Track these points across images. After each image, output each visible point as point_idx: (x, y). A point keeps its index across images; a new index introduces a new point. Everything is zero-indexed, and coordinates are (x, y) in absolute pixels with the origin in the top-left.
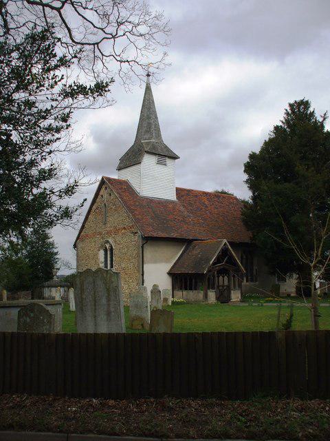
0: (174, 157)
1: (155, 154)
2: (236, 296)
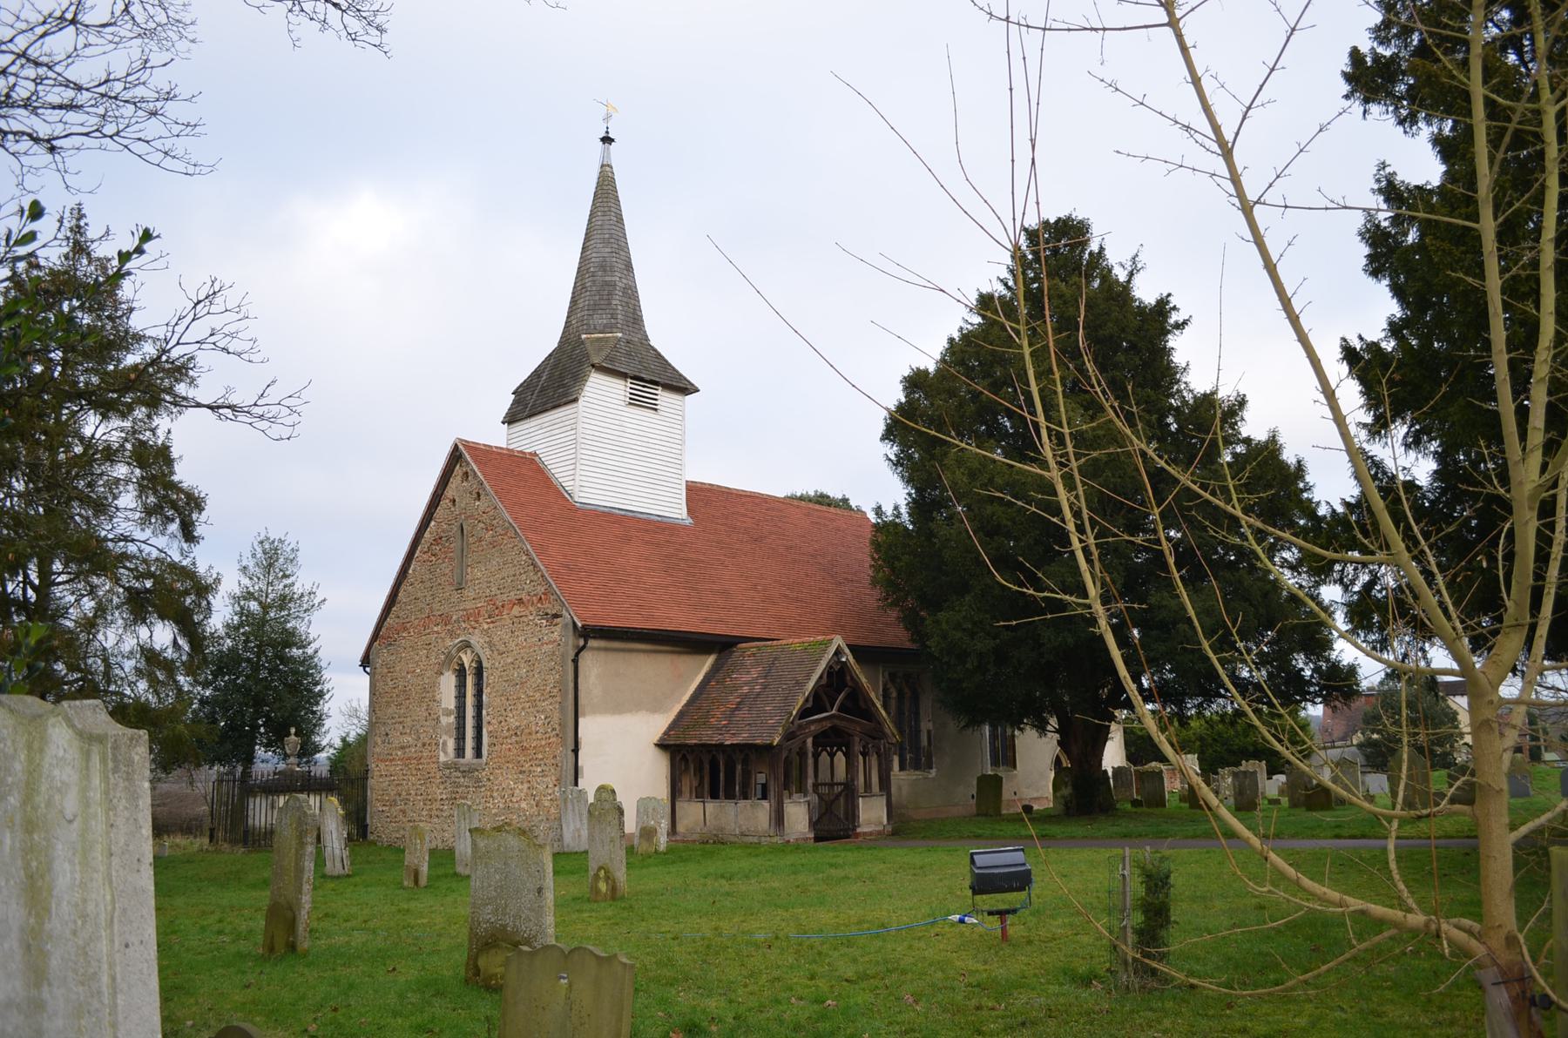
0: (683, 387)
1: (623, 376)
2: (872, 813)
